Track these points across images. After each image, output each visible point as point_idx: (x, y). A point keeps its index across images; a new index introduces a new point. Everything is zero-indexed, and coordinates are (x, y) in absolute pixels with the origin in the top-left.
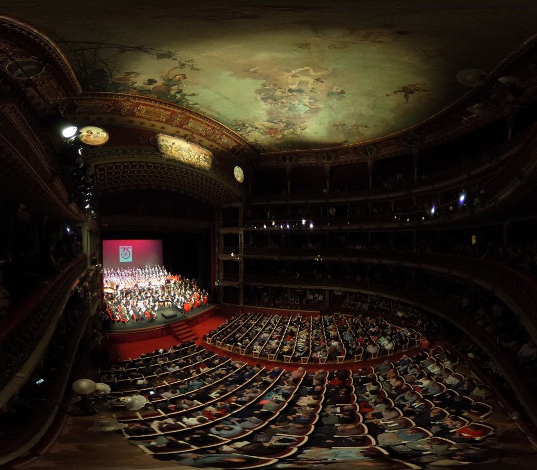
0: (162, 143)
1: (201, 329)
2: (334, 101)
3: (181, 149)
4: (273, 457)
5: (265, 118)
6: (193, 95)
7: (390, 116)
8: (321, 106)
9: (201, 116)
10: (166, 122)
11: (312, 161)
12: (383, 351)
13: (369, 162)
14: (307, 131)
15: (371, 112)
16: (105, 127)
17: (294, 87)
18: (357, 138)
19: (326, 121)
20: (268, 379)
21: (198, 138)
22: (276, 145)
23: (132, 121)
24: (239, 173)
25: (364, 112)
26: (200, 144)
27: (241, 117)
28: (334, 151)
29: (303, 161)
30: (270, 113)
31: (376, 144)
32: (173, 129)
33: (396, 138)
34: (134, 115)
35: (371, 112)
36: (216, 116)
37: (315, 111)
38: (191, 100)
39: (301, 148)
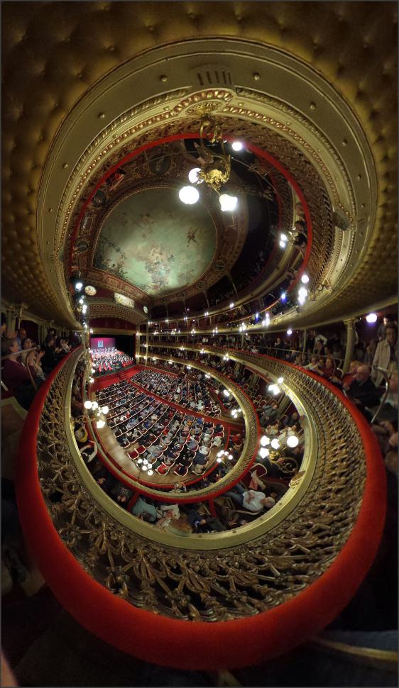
1: (130, 375)
2: (173, 263)
3: (123, 300)
6: (126, 273)
7: (198, 258)
8: (169, 268)
11: (176, 299)
12: (196, 409)
15: (190, 261)
16: (96, 288)
17: (156, 261)
19: (175, 275)
20: (148, 401)
24: (145, 309)
25: (187, 263)
26: (130, 297)
27: (143, 282)
28: (185, 291)
29: (172, 300)
33: (211, 270)
35: (190, 261)
37: (168, 271)
38: (126, 275)
39: (169, 293)
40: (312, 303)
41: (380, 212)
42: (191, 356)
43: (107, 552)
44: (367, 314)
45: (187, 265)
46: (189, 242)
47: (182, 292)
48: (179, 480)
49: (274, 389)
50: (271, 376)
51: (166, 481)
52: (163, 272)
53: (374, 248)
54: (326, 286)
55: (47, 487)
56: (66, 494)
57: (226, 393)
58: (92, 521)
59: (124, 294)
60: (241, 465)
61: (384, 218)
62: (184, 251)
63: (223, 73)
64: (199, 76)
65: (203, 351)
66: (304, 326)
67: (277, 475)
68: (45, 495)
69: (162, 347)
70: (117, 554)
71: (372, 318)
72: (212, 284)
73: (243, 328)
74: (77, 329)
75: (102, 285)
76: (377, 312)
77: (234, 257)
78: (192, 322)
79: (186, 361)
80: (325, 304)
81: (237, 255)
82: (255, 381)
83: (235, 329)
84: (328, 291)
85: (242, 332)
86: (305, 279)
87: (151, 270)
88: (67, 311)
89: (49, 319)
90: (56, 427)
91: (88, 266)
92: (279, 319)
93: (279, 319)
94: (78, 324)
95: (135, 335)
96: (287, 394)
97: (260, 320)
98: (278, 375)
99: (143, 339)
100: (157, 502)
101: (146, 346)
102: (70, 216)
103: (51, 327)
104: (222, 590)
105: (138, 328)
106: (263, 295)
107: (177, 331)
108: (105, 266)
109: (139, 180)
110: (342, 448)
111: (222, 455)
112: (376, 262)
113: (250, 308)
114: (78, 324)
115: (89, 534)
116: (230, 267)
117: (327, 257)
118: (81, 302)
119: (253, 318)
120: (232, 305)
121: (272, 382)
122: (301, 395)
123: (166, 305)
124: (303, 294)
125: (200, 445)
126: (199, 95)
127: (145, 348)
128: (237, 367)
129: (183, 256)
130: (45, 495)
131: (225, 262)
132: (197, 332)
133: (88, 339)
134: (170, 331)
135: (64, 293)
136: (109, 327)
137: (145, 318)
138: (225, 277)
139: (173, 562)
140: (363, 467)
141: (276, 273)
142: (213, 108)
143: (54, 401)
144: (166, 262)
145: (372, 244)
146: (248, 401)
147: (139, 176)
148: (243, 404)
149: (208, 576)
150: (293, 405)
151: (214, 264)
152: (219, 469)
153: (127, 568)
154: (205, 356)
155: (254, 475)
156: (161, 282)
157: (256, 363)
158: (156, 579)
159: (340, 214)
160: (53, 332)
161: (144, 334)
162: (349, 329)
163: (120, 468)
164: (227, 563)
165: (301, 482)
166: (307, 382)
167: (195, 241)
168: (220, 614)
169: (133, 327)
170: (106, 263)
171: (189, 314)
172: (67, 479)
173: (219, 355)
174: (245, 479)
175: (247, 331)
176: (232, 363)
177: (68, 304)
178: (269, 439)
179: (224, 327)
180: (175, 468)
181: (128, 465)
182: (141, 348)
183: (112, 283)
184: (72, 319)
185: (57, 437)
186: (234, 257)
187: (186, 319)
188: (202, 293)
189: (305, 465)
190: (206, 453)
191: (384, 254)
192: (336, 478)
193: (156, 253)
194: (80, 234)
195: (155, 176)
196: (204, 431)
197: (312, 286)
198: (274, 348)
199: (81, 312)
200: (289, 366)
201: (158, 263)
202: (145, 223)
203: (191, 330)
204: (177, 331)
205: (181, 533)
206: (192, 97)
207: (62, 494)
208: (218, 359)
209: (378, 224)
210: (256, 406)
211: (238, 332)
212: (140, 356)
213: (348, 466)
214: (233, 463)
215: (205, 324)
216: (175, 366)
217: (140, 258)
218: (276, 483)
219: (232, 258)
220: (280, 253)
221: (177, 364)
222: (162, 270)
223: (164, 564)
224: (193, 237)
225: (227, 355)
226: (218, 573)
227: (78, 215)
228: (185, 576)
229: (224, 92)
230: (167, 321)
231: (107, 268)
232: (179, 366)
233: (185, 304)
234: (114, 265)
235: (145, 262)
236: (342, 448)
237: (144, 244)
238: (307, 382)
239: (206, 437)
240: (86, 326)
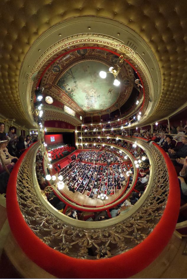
0: (65, 108)
2: (99, 99)
3: (69, 111)
4: (27, 118)
5: (87, 104)
6: (75, 96)
7: (110, 100)
9: (75, 102)
10: (67, 102)
13: (109, 114)
14: (95, 107)
16: (54, 99)
17: (91, 95)
18: (105, 108)
21: (73, 108)
22: (89, 111)
23: (60, 99)
24: (81, 118)
26: (73, 110)
28: (101, 112)
30: (88, 103)
31: (109, 108)
32: (68, 105)
33: (113, 106)
34: (61, 98)
36: (78, 103)
37: (96, 102)
38: (74, 97)
39: (94, 111)
40: (142, 120)
41: (159, 100)
42: (104, 140)
43: (124, 237)
44: (155, 123)
45: (105, 101)
46: (108, 93)
47: (100, 112)
48: (120, 191)
49: (134, 146)
50: (133, 142)
51: (117, 196)
52: (93, 101)
53: (157, 108)
54: (145, 116)
55: (63, 249)
56: (80, 242)
57: (120, 152)
58: (105, 236)
59: (70, 107)
60: (136, 172)
61: (160, 102)
62: (105, 95)
63: (135, 46)
64: (129, 42)
65: (108, 138)
66: (140, 126)
67: (145, 168)
68: (67, 254)
69: (94, 137)
70: (127, 233)
71: (157, 124)
72: (113, 111)
73: (122, 128)
74: (35, 128)
75: (58, 98)
76: (158, 122)
77: (123, 104)
78: (103, 126)
79: (102, 143)
80: (145, 120)
81: (124, 103)
82: (129, 145)
83: (119, 128)
84: (146, 117)
85: (122, 129)
86: (140, 113)
87: (87, 99)
88: (28, 113)
89: (11, 118)
90: (37, 210)
91: (54, 83)
92: (133, 124)
93: (133, 124)
94: (35, 124)
95: (74, 132)
96: (139, 146)
97: (127, 125)
98: (135, 141)
99: (79, 134)
100: (118, 206)
101: (81, 138)
102: (63, 49)
103: (13, 125)
104: (159, 201)
105: (76, 128)
106: (129, 117)
107: (96, 129)
108: (63, 87)
109: (105, 58)
110: (156, 154)
111: (128, 173)
112: (158, 111)
113: (126, 120)
114: (35, 124)
115: (110, 241)
116: (120, 107)
117: (147, 108)
118: (36, 110)
119: (125, 124)
120: (119, 120)
121: (133, 144)
122: (142, 145)
123: (92, 117)
124: (139, 117)
125: (119, 174)
126: (125, 46)
127: (80, 139)
128: (122, 141)
129: (104, 97)
130: (67, 254)
131: (119, 104)
132: (105, 130)
133: (43, 135)
134: (93, 130)
135: (28, 99)
136: (58, 127)
137: (80, 123)
138: (118, 110)
139: (143, 211)
140: (163, 156)
141: (134, 111)
142: (127, 53)
143: (25, 191)
144: (96, 97)
145: (157, 107)
146: (129, 152)
147: (106, 57)
148: (127, 153)
149: (154, 202)
150: (142, 149)
151: (115, 104)
152: (130, 179)
153: (152, 213)
154: (109, 139)
155: (141, 173)
156: (91, 106)
157: (128, 139)
158: (146, 220)
159: (151, 98)
160: (13, 131)
161: (80, 132)
162: (152, 126)
163: (95, 207)
164: (153, 195)
165: (152, 168)
166: (143, 141)
167: (111, 93)
168: (165, 204)
169: (73, 127)
170: (65, 86)
171: (102, 122)
172: (72, 234)
173: (115, 138)
174: (139, 175)
175: (123, 129)
176: (120, 141)
177: (30, 108)
178: (137, 161)
179: (116, 128)
180: (116, 189)
181: (98, 202)
182: (78, 139)
183: (64, 99)
184: (30, 119)
185: (43, 216)
186: (123, 104)
187: (100, 124)
188: (108, 114)
189: (151, 163)
190: (123, 175)
191: (159, 109)
192: (159, 162)
193: (93, 91)
194: (59, 61)
195: (111, 62)
196: (118, 168)
197: (142, 115)
198: (132, 132)
199: (38, 116)
200: (137, 138)
201: (92, 96)
202: (94, 76)
203: (102, 129)
204: (96, 129)
205: (126, 211)
206: (122, 46)
207: (77, 244)
208: (115, 140)
209: (158, 103)
210: (131, 153)
211: (121, 129)
212: (79, 144)
213: (160, 158)
214: (133, 173)
215: (108, 126)
216: (98, 146)
217: (84, 91)
218: (147, 171)
219: (122, 104)
220: (136, 106)
221: (98, 145)
222: (93, 99)
223: (125, 228)
224: (111, 91)
225: (117, 138)
226: (154, 199)
227: (66, 52)
228: (149, 210)
229: (132, 51)
230: (92, 125)
231: (65, 89)
232: (99, 145)
233: (100, 118)
234: (69, 89)
235: (86, 94)
236: (156, 154)
237: (89, 85)
238: (143, 141)
239: (120, 170)
240: (41, 126)
